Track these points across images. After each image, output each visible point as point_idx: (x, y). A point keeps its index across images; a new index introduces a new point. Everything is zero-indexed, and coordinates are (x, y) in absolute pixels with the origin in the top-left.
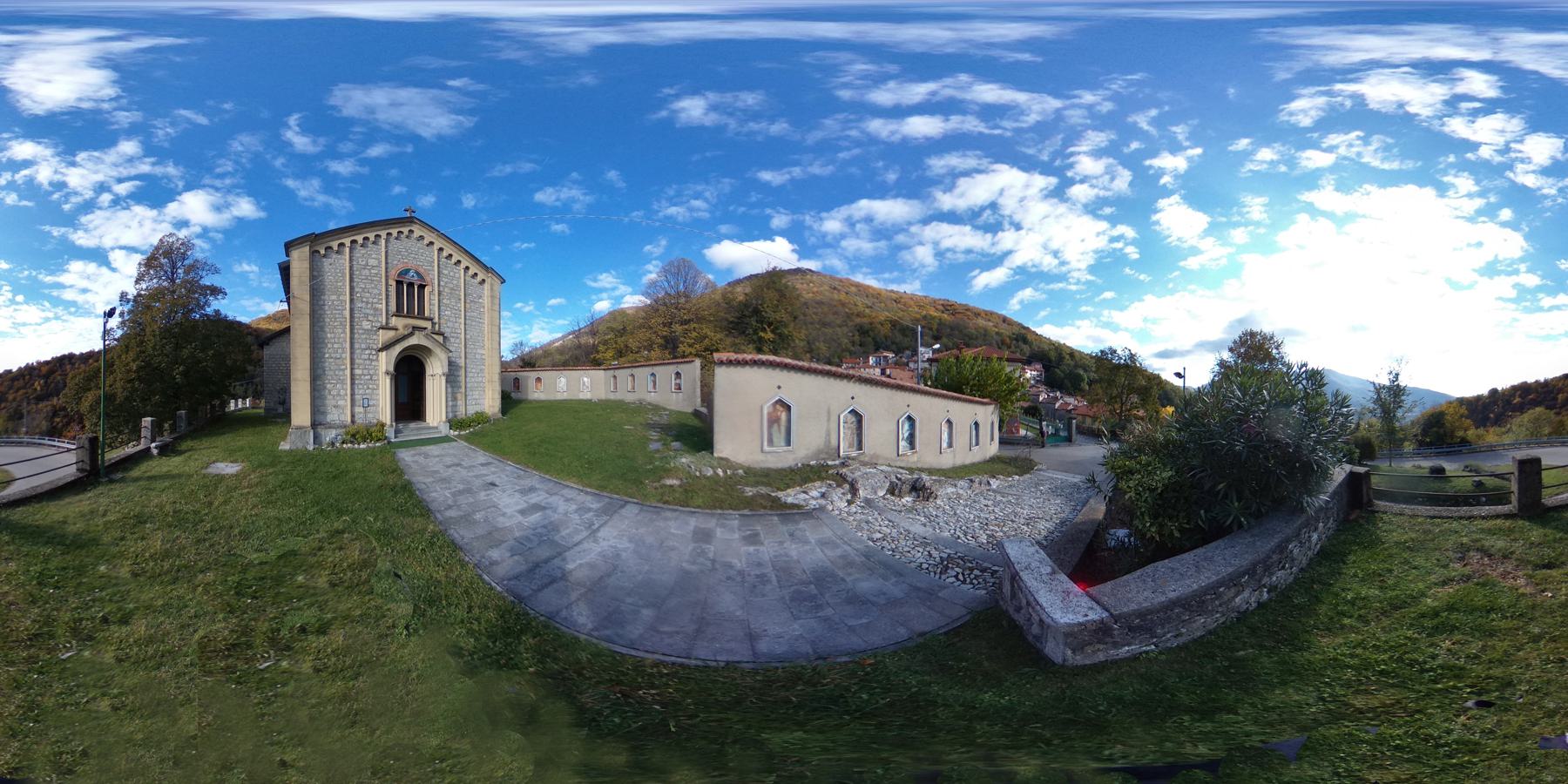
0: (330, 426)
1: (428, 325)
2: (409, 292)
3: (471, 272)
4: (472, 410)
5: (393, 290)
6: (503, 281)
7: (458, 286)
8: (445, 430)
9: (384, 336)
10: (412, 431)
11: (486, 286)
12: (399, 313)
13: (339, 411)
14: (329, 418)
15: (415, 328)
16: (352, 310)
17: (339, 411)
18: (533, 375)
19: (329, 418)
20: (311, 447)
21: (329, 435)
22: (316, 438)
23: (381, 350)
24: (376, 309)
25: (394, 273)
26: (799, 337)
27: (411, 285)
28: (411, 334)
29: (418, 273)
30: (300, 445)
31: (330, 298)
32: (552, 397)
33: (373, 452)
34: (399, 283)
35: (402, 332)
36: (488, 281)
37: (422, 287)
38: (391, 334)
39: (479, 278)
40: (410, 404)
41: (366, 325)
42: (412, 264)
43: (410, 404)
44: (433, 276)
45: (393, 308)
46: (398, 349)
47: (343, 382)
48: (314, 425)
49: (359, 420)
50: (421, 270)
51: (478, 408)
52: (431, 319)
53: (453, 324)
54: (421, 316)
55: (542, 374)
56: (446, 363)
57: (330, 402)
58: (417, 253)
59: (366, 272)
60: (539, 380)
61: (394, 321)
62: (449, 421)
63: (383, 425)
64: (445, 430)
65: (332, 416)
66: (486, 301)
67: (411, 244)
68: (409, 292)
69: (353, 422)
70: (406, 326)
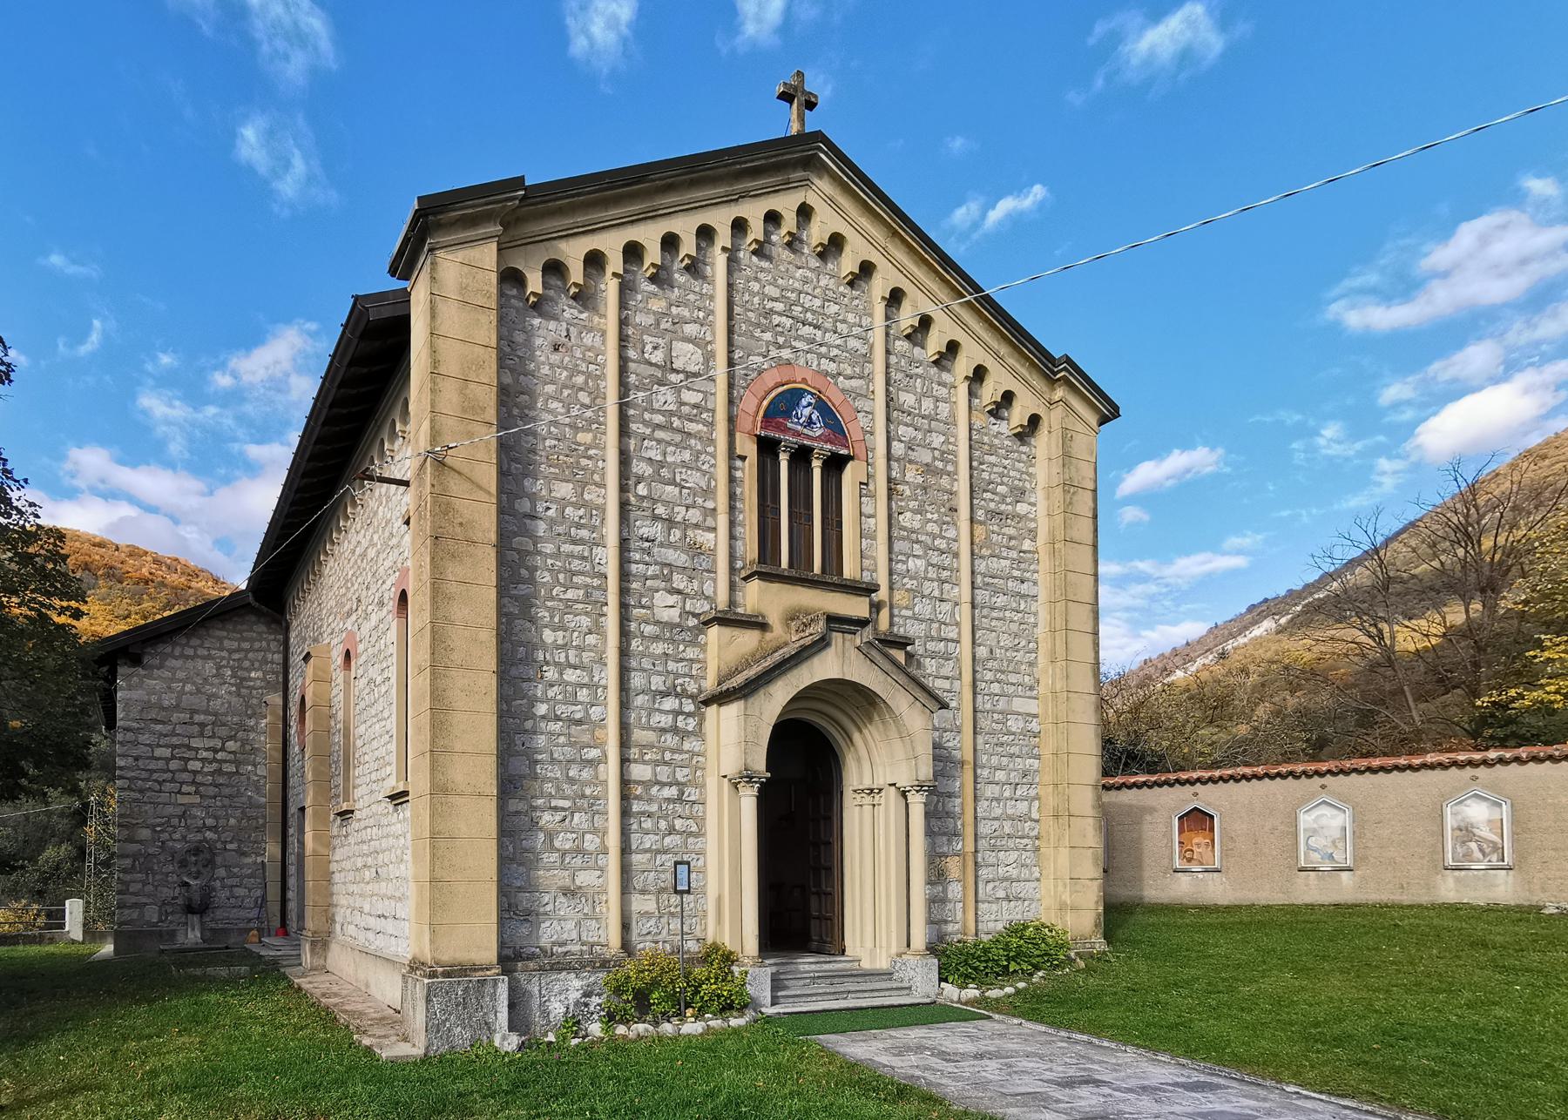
0: (560, 965)
1: (856, 607)
2: (797, 460)
3: (990, 392)
4: (995, 920)
5: (748, 472)
6: (1109, 412)
7: (947, 455)
8: (922, 981)
9: (721, 651)
10: (810, 984)
11: (1043, 443)
12: (767, 570)
13: (586, 911)
14: (548, 934)
15: (835, 621)
16: (624, 545)
17: (586, 911)
18: (1169, 802)
19: (548, 934)
20: (508, 1042)
21: (560, 996)
22: (517, 1003)
23: (722, 698)
24: (695, 550)
25: (752, 406)
26: (514, 805)
27: (801, 456)
28: (822, 643)
29: (822, 407)
30: (461, 1036)
31: (553, 491)
32: (1266, 893)
33: (710, 1045)
34: (767, 448)
35: (791, 639)
36: (1053, 420)
37: (835, 465)
38: (748, 640)
39: (1018, 415)
40: (800, 899)
41: (665, 607)
42: (807, 368)
43: (800, 899)
44: (868, 422)
45: (749, 547)
46: (779, 695)
47: (593, 807)
48: (510, 958)
49: (643, 946)
50: (834, 397)
51: (1014, 913)
52: (868, 590)
53: (934, 613)
54: (831, 580)
55: (1209, 797)
56: (925, 752)
57: (550, 875)
58: (804, 306)
59: (665, 397)
60: (1197, 820)
61: (755, 596)
62: (934, 948)
63: (729, 959)
64: (922, 981)
65: (559, 928)
66: (1040, 508)
67: (792, 278)
68: (797, 460)
69: (626, 946)
70: (791, 617)
